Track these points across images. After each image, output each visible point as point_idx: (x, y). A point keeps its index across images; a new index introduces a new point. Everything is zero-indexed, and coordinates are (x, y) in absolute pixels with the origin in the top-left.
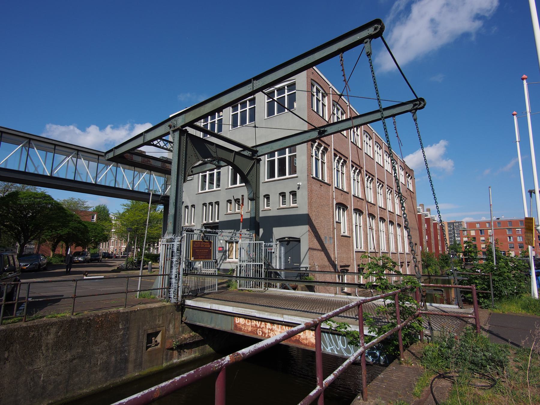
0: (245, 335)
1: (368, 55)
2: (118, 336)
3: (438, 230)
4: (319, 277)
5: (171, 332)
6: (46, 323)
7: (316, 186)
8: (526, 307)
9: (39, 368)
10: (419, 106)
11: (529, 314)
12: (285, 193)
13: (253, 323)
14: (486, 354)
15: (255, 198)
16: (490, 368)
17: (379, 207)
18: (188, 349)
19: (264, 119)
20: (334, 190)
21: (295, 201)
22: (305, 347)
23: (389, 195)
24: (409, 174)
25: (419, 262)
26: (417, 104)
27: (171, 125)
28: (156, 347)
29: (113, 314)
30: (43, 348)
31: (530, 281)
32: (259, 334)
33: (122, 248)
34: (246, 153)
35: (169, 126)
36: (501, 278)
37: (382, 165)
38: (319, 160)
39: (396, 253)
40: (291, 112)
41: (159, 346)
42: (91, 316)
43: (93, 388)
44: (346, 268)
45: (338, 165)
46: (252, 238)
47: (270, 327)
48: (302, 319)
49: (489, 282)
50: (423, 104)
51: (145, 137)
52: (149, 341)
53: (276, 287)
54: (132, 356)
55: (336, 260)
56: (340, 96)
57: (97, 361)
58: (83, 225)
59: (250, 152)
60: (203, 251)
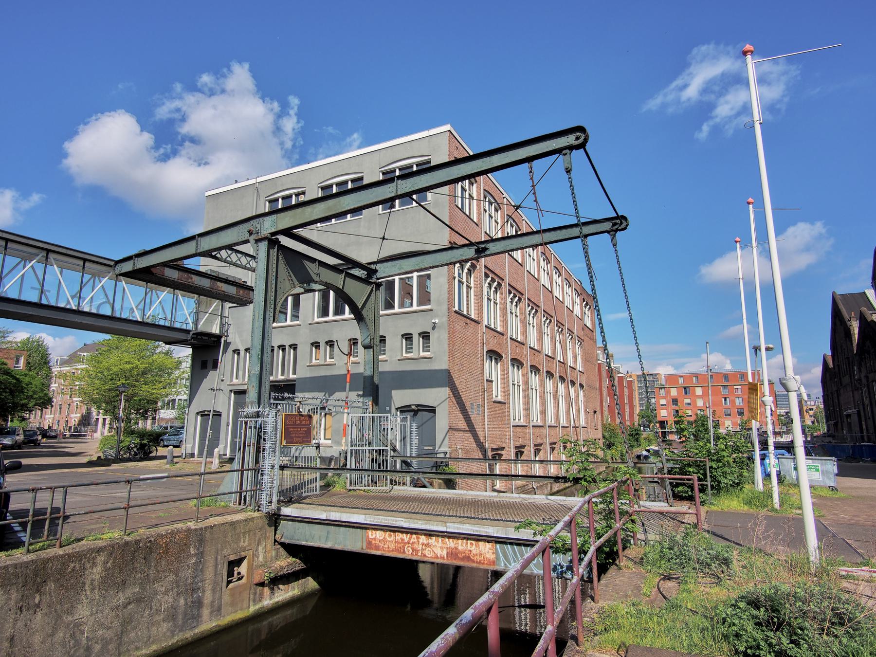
0: (386, 555)
1: (567, 172)
2: (188, 566)
3: (625, 388)
4: (462, 467)
5: (261, 558)
6: (91, 549)
7: (460, 322)
8: (749, 502)
9: (81, 618)
10: (620, 226)
11: (752, 510)
12: (412, 334)
13: (397, 537)
14: (710, 552)
15: (373, 345)
16: (715, 567)
17: (511, 338)
18: (284, 584)
19: (377, 213)
20: (484, 331)
21: (427, 348)
22: (478, 565)
25: (599, 439)
26: (618, 224)
27: (253, 231)
28: (240, 581)
29: (181, 532)
30: (87, 587)
31: (754, 468)
32: (407, 552)
33: (71, 418)
34: (357, 272)
35: (249, 232)
36: (720, 464)
37: (536, 276)
38: (463, 284)
39: (568, 427)
40: (422, 206)
41: (244, 580)
42: (152, 536)
43: (154, 647)
44: (499, 452)
45: (461, 272)
46: (368, 407)
47: (425, 542)
48: (475, 527)
49: (705, 470)
50: (625, 224)
51: (199, 243)
52: (230, 574)
53: (404, 484)
54: (208, 597)
56: (517, 207)
57: (161, 606)
58: (15, 378)
59: (364, 272)
60: (299, 429)
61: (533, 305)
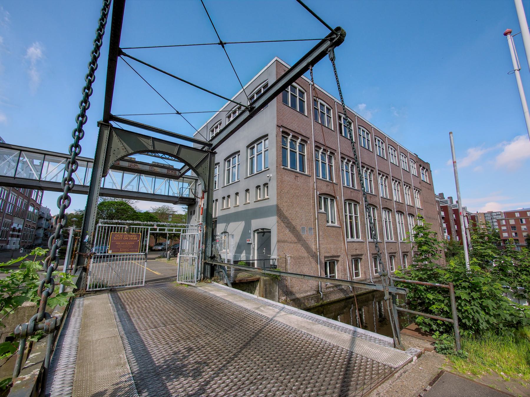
17: (417, 208)
20: (315, 181)
23: (417, 194)
24: (423, 167)
55: (318, 250)
61: (349, 158)
